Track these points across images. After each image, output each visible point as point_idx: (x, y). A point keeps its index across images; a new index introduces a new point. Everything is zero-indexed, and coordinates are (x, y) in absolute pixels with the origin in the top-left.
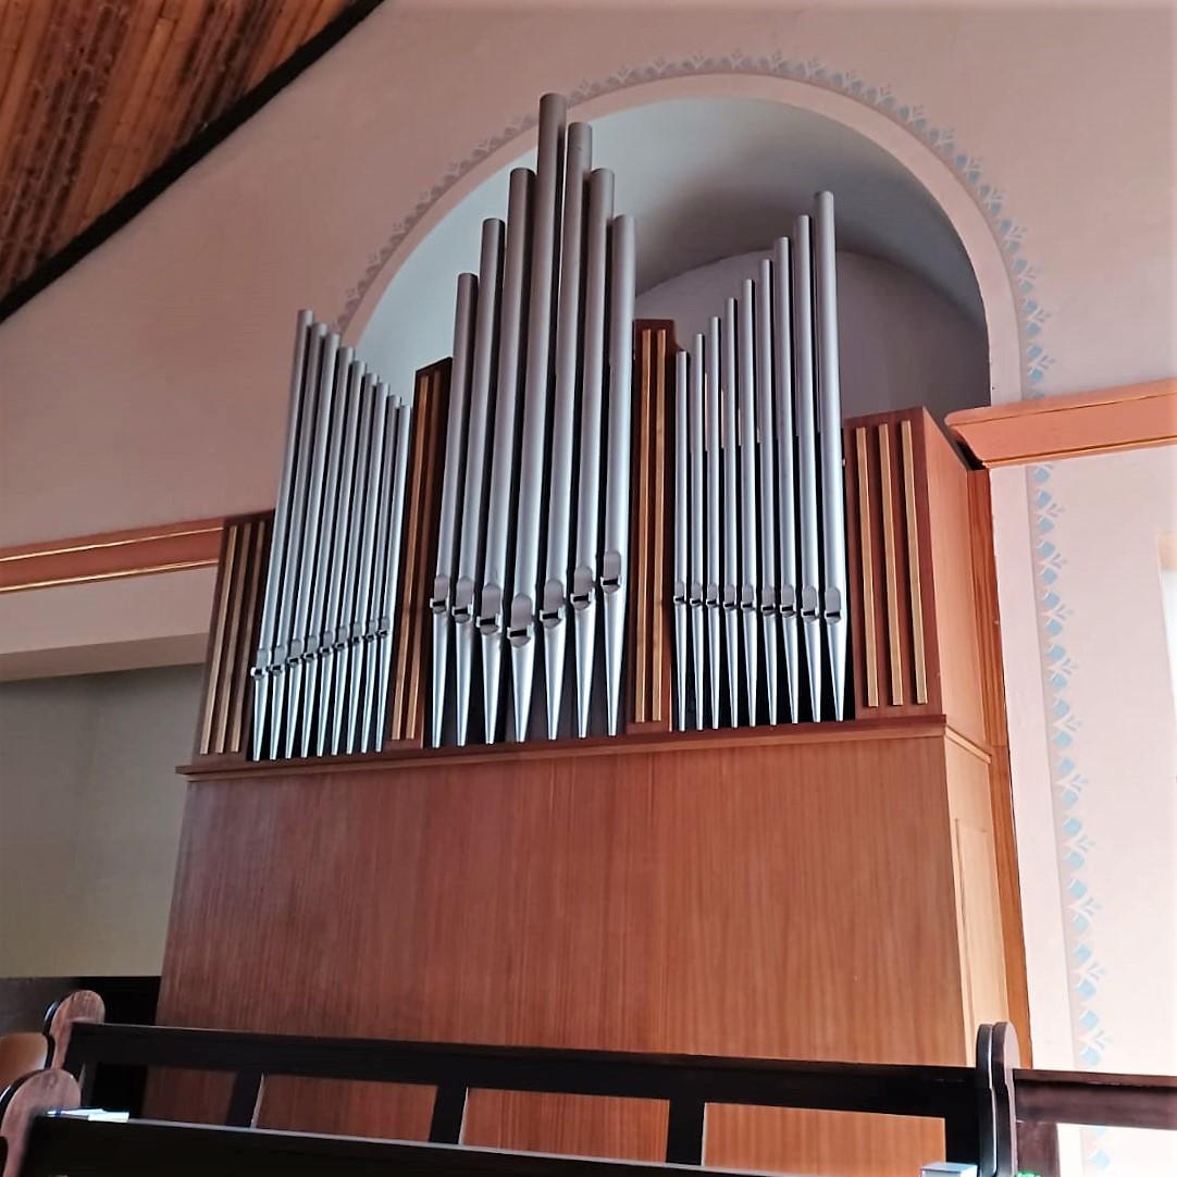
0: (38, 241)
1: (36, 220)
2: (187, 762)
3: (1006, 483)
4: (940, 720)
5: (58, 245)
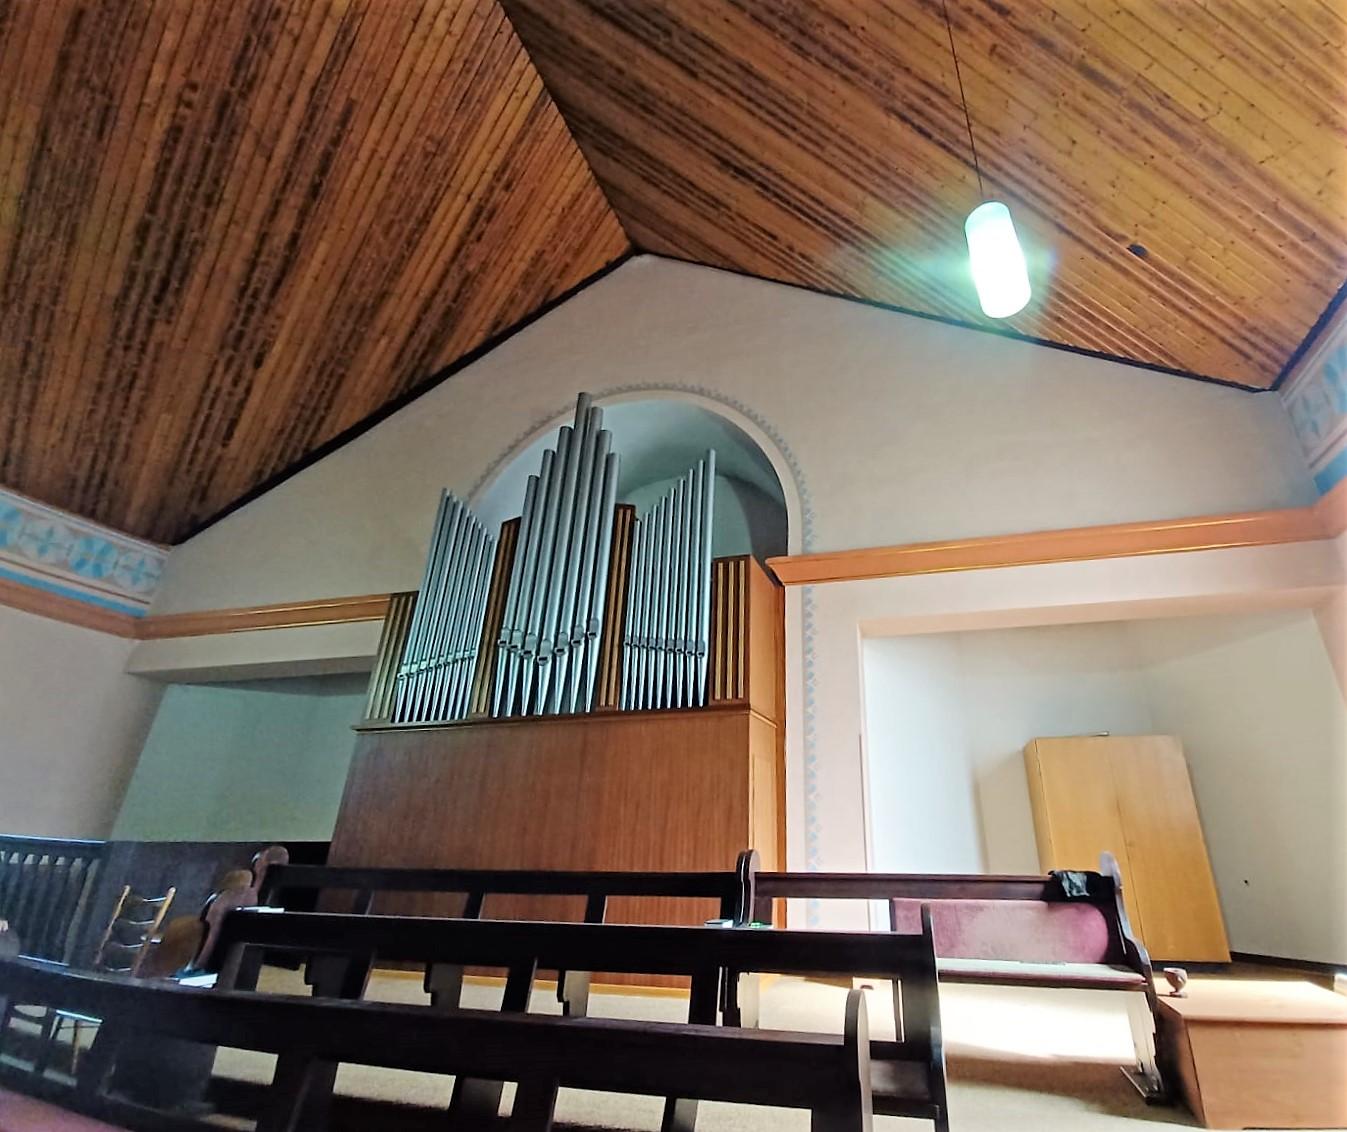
0: (305, 442)
1: (304, 432)
2: (358, 724)
3: (792, 593)
4: (746, 706)
5: (314, 447)
